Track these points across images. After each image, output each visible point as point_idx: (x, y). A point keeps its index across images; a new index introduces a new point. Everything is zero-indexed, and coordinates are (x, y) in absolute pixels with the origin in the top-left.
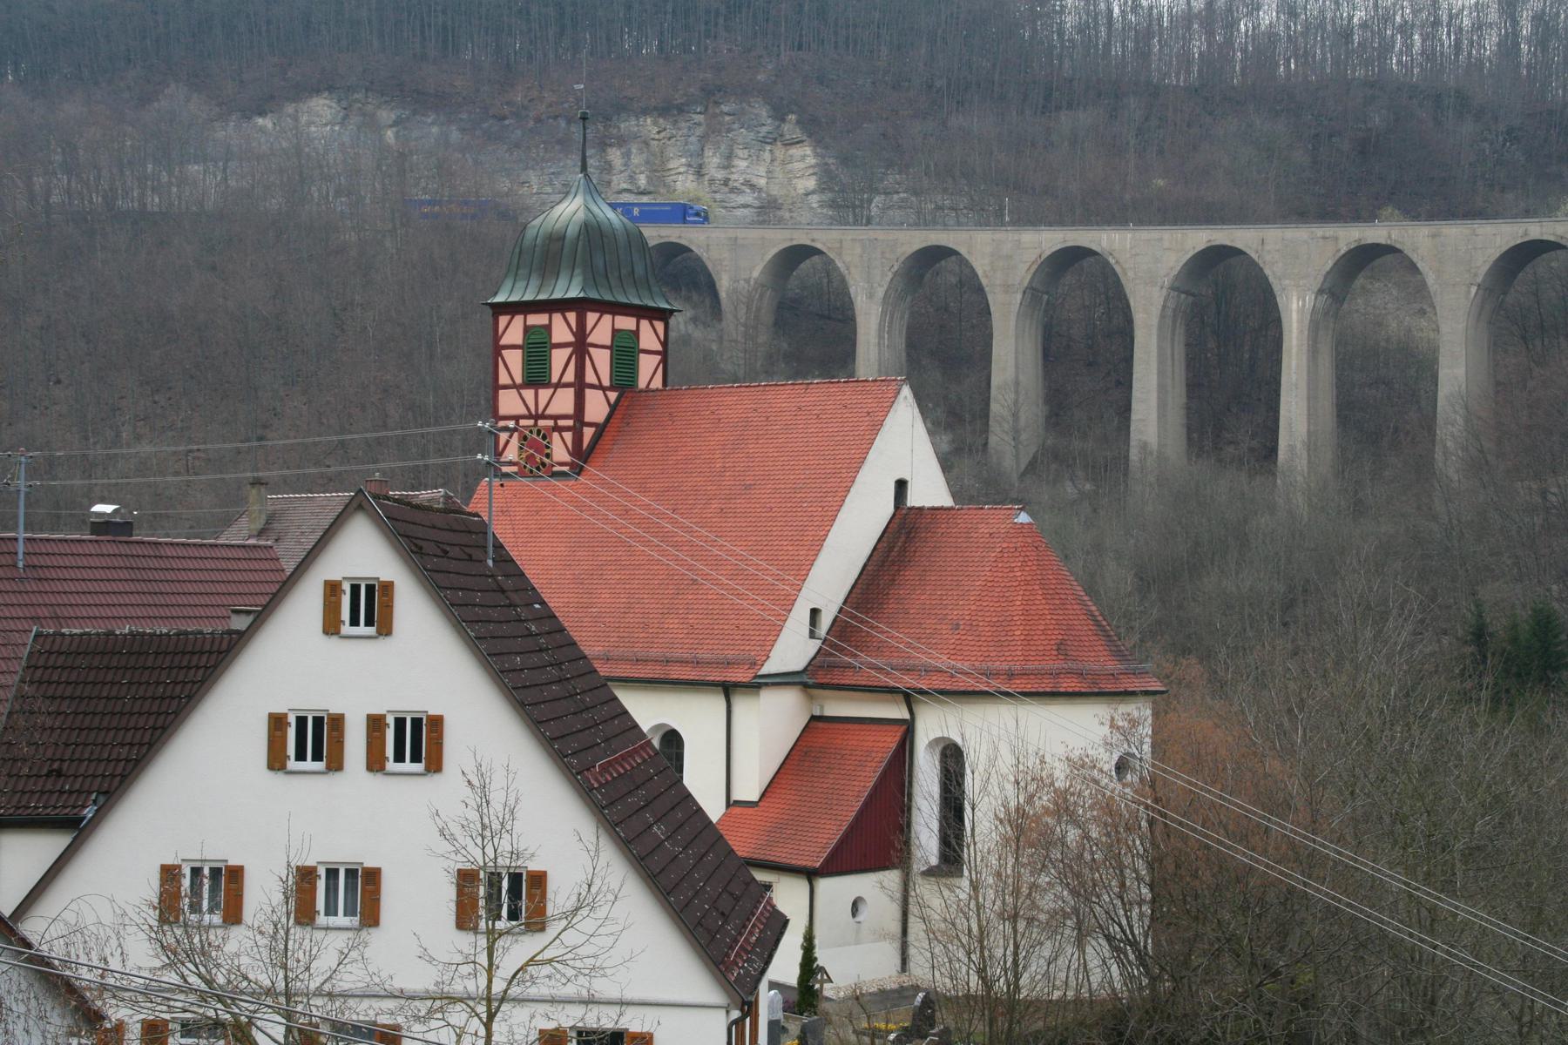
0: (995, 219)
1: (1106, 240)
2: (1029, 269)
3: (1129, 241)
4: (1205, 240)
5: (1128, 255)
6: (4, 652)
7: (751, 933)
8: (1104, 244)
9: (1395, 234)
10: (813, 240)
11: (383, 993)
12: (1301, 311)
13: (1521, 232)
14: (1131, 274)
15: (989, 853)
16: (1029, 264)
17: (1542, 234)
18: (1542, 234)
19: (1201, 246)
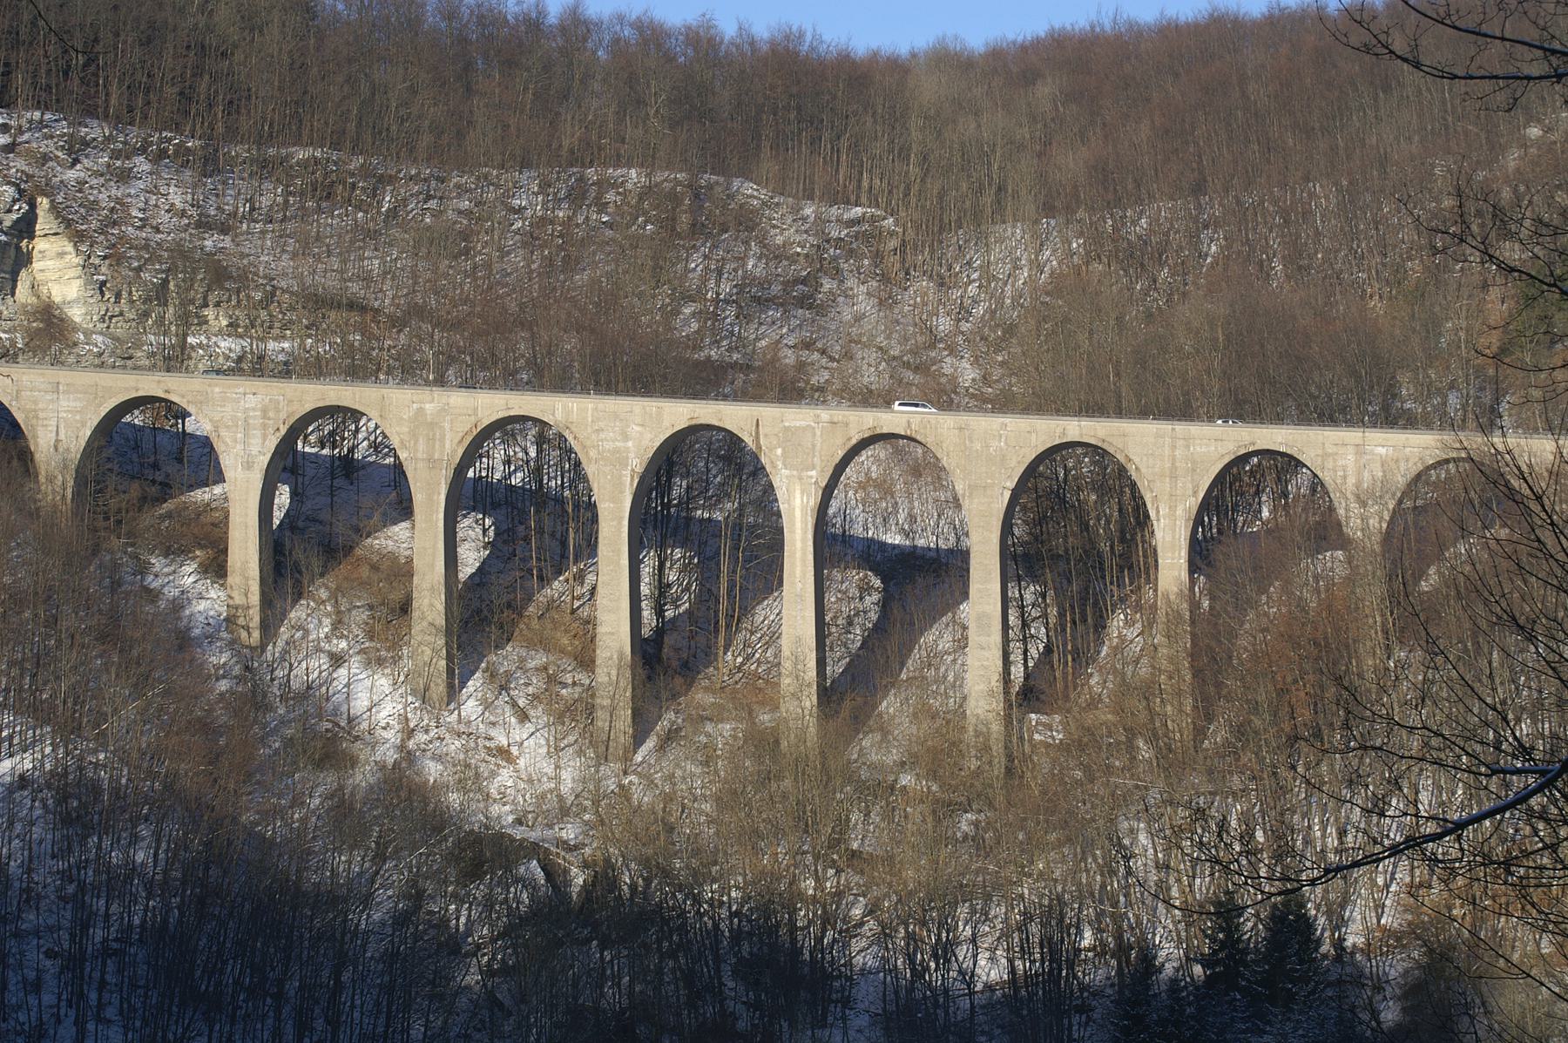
0: (407, 371)
1: (732, 416)
2: (461, 442)
3: (590, 412)
4: (686, 417)
5: (589, 430)
6: (389, 1042)
7: (1376, 633)
8: (559, 415)
9: (916, 421)
10: (167, 391)
11: (1435, 16)
12: (804, 508)
13: (1059, 430)
14: (593, 453)
15: (1383, 689)
16: (461, 434)
17: (1081, 435)
18: (1081, 435)
19: (682, 424)
